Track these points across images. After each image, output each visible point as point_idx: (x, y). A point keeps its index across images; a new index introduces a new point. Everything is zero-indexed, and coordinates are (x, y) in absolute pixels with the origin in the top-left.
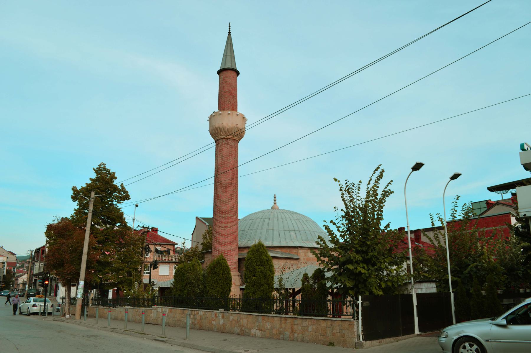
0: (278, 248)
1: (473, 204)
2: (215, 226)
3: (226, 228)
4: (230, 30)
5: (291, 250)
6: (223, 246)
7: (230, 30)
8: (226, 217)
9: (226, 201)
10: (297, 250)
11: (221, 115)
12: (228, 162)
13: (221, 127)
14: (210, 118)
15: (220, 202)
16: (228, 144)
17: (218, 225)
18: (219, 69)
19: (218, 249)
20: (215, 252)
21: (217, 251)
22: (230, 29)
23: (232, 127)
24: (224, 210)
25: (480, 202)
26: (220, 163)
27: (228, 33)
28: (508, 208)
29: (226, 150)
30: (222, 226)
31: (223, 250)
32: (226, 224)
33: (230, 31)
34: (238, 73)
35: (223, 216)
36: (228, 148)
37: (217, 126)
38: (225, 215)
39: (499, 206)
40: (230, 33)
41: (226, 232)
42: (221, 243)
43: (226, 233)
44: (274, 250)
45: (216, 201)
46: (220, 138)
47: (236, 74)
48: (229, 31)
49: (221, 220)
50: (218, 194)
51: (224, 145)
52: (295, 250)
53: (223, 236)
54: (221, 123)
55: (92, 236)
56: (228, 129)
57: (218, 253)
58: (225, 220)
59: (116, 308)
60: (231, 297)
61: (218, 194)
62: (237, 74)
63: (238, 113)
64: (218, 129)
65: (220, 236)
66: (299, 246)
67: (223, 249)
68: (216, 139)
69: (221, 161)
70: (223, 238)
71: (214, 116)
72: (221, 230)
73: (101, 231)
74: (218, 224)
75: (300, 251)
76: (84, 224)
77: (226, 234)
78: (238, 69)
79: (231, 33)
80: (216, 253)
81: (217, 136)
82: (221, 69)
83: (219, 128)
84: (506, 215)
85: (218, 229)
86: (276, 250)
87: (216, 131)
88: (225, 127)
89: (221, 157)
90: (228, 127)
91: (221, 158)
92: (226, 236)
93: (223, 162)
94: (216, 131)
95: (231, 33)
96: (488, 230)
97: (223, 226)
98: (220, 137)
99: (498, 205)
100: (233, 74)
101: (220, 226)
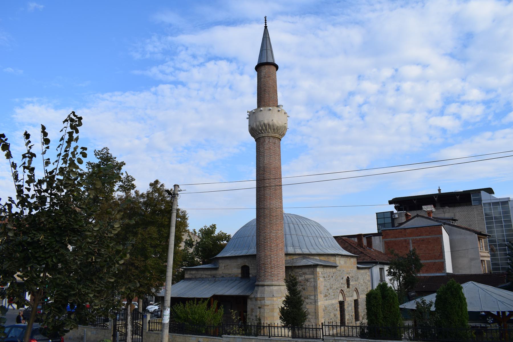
0: (317, 256)
1: (378, 214)
3: (277, 234)
4: (266, 24)
5: (329, 257)
7: (266, 24)
10: (335, 257)
11: (270, 111)
12: (276, 163)
13: (271, 123)
15: (270, 204)
16: (275, 143)
18: (257, 64)
20: (266, 261)
21: (269, 259)
23: (281, 125)
25: (384, 212)
26: (268, 162)
27: (265, 27)
28: (427, 220)
29: (273, 149)
31: (275, 258)
32: (277, 229)
33: (267, 25)
35: (274, 220)
37: (266, 122)
38: (276, 220)
39: (419, 217)
40: (266, 27)
42: (273, 250)
43: (277, 239)
44: (312, 257)
45: (265, 203)
46: (267, 135)
47: (275, 69)
48: (265, 25)
49: (271, 225)
50: (267, 196)
51: (271, 143)
54: (270, 120)
56: (277, 127)
57: (269, 262)
58: (276, 225)
60: (363, 324)
61: (267, 196)
62: (276, 68)
66: (338, 254)
67: (275, 257)
68: (257, 138)
69: (268, 160)
70: (275, 245)
71: (254, 113)
73: (420, 263)
75: (337, 258)
77: (278, 241)
81: (263, 133)
83: (269, 125)
84: (437, 226)
85: (268, 235)
86: (315, 258)
87: (264, 128)
88: (276, 125)
90: (278, 126)
91: (268, 157)
92: (277, 242)
93: (271, 161)
94: (264, 128)
96: (421, 238)
98: (267, 134)
99: (418, 217)
100: (274, 68)
101: (271, 232)
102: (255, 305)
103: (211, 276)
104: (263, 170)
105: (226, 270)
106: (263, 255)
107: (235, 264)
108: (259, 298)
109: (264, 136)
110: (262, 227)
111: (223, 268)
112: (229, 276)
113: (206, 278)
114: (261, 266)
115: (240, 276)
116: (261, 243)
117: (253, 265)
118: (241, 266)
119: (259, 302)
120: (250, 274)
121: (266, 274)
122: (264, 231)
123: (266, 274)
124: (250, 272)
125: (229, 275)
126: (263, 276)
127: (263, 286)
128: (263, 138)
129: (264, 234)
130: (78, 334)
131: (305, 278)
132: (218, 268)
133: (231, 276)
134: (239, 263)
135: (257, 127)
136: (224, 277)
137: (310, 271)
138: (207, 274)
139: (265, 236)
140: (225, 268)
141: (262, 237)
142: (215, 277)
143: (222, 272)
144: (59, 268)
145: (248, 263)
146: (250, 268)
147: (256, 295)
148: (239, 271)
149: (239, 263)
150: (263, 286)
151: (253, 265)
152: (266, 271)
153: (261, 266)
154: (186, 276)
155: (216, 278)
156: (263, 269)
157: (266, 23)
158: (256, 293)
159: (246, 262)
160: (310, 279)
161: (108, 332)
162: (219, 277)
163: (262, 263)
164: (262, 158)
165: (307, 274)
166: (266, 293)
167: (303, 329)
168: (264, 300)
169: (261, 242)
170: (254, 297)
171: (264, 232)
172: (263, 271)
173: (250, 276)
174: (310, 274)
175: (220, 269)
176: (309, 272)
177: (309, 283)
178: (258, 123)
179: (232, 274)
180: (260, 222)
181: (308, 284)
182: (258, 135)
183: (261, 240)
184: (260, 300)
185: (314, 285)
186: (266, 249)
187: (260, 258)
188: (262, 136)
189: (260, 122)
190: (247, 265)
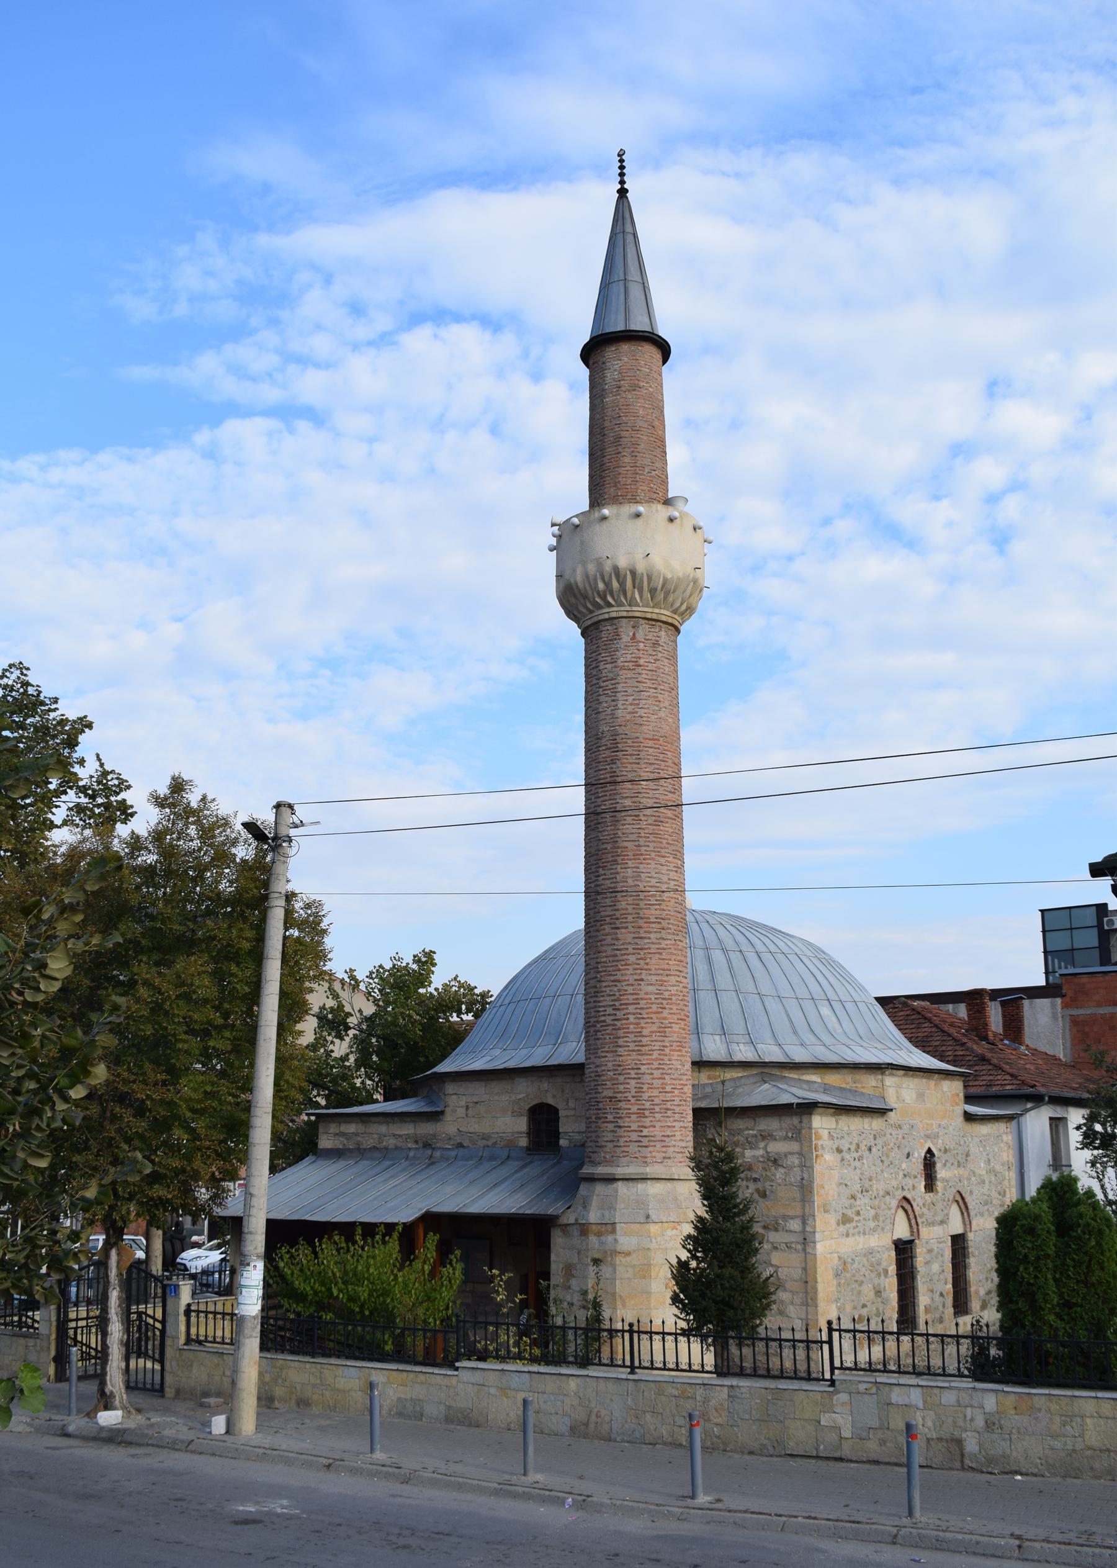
0: (812, 1071)
2: (612, 978)
4: (622, 182)
5: (857, 1077)
6: (657, 1059)
7: (622, 182)
8: (664, 944)
9: (661, 876)
10: (880, 1077)
11: (639, 522)
14: (560, 536)
17: (628, 972)
19: (632, 1072)
21: (633, 1082)
22: (625, 178)
24: (653, 912)
26: (628, 717)
27: (618, 191)
30: (649, 978)
33: (626, 186)
34: (665, 350)
36: (656, 660)
37: (623, 563)
38: (659, 936)
40: (623, 192)
41: (665, 1002)
42: (647, 1048)
44: (796, 1076)
46: (625, 614)
48: (619, 186)
50: (625, 844)
51: (642, 645)
52: (872, 1077)
53: (655, 1020)
55: (1042, 1191)
56: (665, 581)
58: (660, 954)
59: (457, 1369)
61: (625, 844)
63: (677, 514)
64: (625, 576)
65: (642, 1021)
69: (630, 708)
71: (577, 526)
72: (647, 993)
74: (630, 967)
75: (891, 1081)
76: (1098, 1128)
77: (665, 1013)
78: (663, 332)
79: (627, 191)
80: (628, 1091)
82: (594, 335)
83: (633, 573)
85: (630, 989)
89: (630, 690)
91: (631, 698)
94: (615, 584)
95: (627, 191)
97: (654, 978)
98: (628, 608)
100: (651, 353)
101: (642, 980)
102: (579, 1253)
103: (416, 1142)
105: (474, 1120)
107: (505, 1097)
108: (594, 1227)
110: (604, 960)
111: (461, 1112)
112: (485, 1142)
113: (396, 1148)
114: (601, 1106)
115: (524, 1142)
116: (604, 1021)
117: (571, 1104)
118: (527, 1107)
119: (593, 1239)
124: (561, 1130)
125: (483, 1139)
126: (610, 1145)
131: (767, 1152)
132: (442, 1113)
133: (490, 1143)
134: (521, 1096)
137: (784, 1125)
138: (400, 1136)
139: (617, 994)
140: (467, 1115)
145: (554, 1096)
146: (562, 1113)
148: (522, 1124)
151: (571, 1104)
153: (601, 1106)
154: (325, 1142)
155: (434, 1149)
156: (610, 1117)
159: (547, 1091)
160: (786, 1156)
162: (447, 1146)
165: (775, 1140)
166: (620, 1205)
168: (614, 1231)
170: (576, 1223)
172: (611, 1126)
173: (563, 1142)
174: (786, 1138)
175: (448, 1117)
176: (781, 1129)
177: (781, 1170)
182: (591, 612)
183: (601, 1009)
184: (599, 1234)
185: (802, 1179)
188: (606, 616)
190: (550, 1101)
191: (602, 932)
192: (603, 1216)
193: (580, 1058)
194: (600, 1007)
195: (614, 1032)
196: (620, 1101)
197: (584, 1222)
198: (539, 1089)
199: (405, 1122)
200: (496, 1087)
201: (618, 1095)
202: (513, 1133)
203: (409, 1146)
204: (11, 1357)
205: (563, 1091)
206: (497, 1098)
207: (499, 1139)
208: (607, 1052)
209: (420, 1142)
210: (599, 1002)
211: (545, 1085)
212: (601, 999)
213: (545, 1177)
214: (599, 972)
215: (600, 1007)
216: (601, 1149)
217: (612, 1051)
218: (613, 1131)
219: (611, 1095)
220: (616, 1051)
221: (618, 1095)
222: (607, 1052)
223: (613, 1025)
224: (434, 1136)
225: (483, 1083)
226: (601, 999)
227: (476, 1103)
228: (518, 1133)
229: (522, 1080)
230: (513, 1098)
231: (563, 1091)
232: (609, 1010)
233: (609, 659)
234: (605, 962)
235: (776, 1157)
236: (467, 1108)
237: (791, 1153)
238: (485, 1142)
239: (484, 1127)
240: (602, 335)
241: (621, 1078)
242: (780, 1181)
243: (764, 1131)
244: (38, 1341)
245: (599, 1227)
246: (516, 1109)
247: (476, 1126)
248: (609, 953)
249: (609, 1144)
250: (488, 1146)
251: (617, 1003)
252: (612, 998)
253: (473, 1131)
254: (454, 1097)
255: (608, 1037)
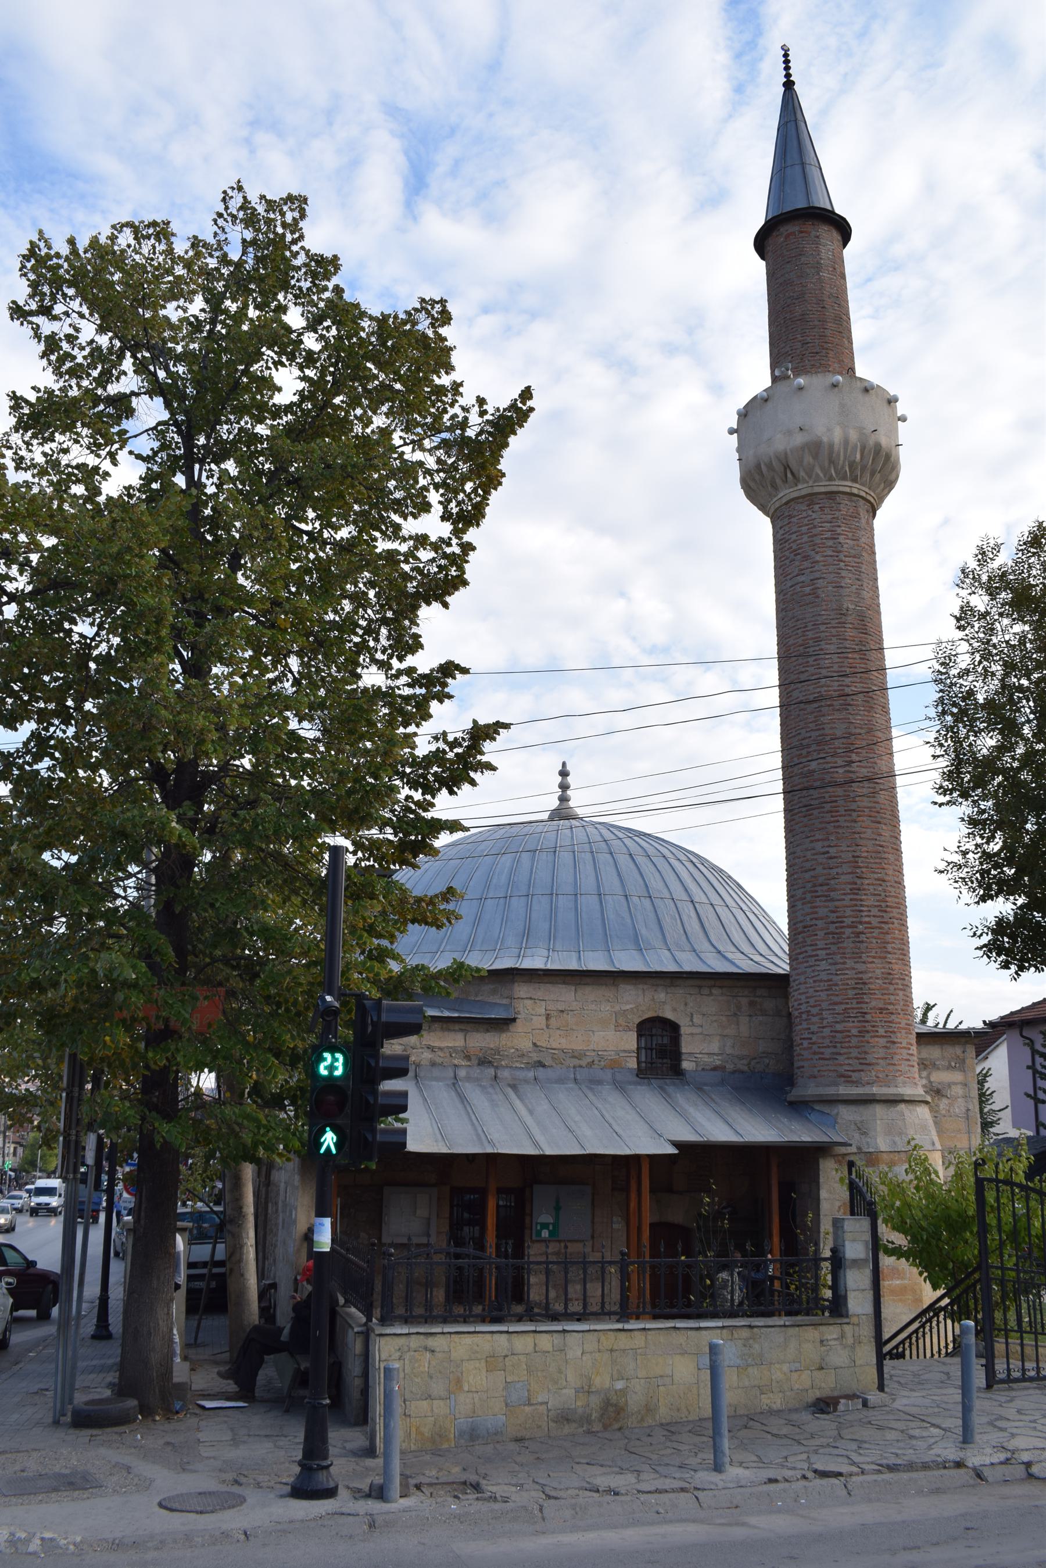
21: (901, 993)
27: (784, 85)
40: (789, 85)
98: (867, 490)
103: (468, 1058)
104: (856, 626)
105: (558, 1032)
106: (878, 972)
107: (606, 1007)
108: (885, 1156)
109: (855, 491)
110: (865, 854)
111: (540, 1022)
112: (577, 1062)
113: (433, 1064)
114: (868, 1017)
115: (633, 1064)
116: (869, 923)
117: (697, 1019)
118: (637, 1021)
120: (683, 1057)
121: (895, 1053)
122: (876, 876)
123: (895, 1053)
124: (684, 1050)
125: (574, 1057)
127: (893, 1101)
128: (851, 501)
129: (880, 888)
130: (570, 1392)
131: (930, 1082)
132: (514, 1020)
133: (583, 1063)
134: (628, 1007)
135: (846, 450)
136: (544, 1066)
138: (440, 1049)
139: (883, 894)
140: (548, 1026)
141: (871, 901)
142: (490, 1062)
143: (534, 1044)
144: (46, 864)
145: (674, 1010)
146: (684, 1030)
147: (868, 1143)
148: (630, 1041)
149: (627, 1003)
150: (893, 1101)
151: (697, 1019)
152: (894, 1043)
153: (868, 1017)
155: (497, 1068)
156: (881, 1031)
157: (784, 73)
158: (865, 1134)
159: (664, 1003)
161: (850, 1341)
162: (518, 1065)
163: (874, 1008)
164: (850, 575)
165: (938, 1069)
167: (1007, 1278)
169: (867, 919)
171: (878, 879)
172: (882, 1041)
173: (686, 1065)
174: (949, 1068)
175: (519, 1027)
176: (943, 1058)
177: (945, 1101)
178: (853, 436)
179: (593, 1054)
180: (857, 836)
181: (942, 1107)
182: (831, 479)
185: (968, 1110)
186: (890, 950)
187: (865, 983)
188: (848, 490)
189: (861, 430)
190: (669, 1015)
191: (859, 824)
192: (895, 1143)
193: (783, 967)
194: (862, 905)
195: (882, 936)
196: (892, 1013)
197: (871, 1150)
198: (653, 1000)
199: (449, 1030)
200: (590, 994)
201: (890, 1007)
202: (617, 1053)
203: (456, 1062)
204: (785, 1368)
205: (686, 1004)
206: (593, 1007)
207: (596, 1059)
208: (874, 957)
209: (473, 1058)
210: (861, 900)
211: (661, 996)
212: (864, 897)
213: (686, 1107)
214: (860, 867)
215: (862, 905)
216: (871, 1068)
217: (880, 957)
218: (886, 1047)
219: (881, 1006)
220: (885, 958)
221: (890, 1007)
222: (874, 957)
223: (880, 928)
224: (497, 1051)
225: (573, 988)
226: (864, 897)
227: (562, 1011)
228: (625, 1051)
229: (628, 987)
230: (617, 1008)
231: (686, 1004)
232: (875, 911)
233: (850, 535)
234: (866, 857)
235: (940, 1087)
236: (548, 1017)
237: (955, 1084)
238: (577, 1062)
239: (576, 1043)
240: (782, 214)
241: (892, 987)
242: (944, 1112)
243: (926, 1059)
244: (846, 1328)
245: (892, 1155)
246: (620, 1021)
247: (563, 1041)
248: (871, 849)
249: (880, 1061)
250: (581, 1066)
251: (883, 904)
252: (878, 898)
253: (559, 1046)
254: (528, 1002)
255: (874, 941)
